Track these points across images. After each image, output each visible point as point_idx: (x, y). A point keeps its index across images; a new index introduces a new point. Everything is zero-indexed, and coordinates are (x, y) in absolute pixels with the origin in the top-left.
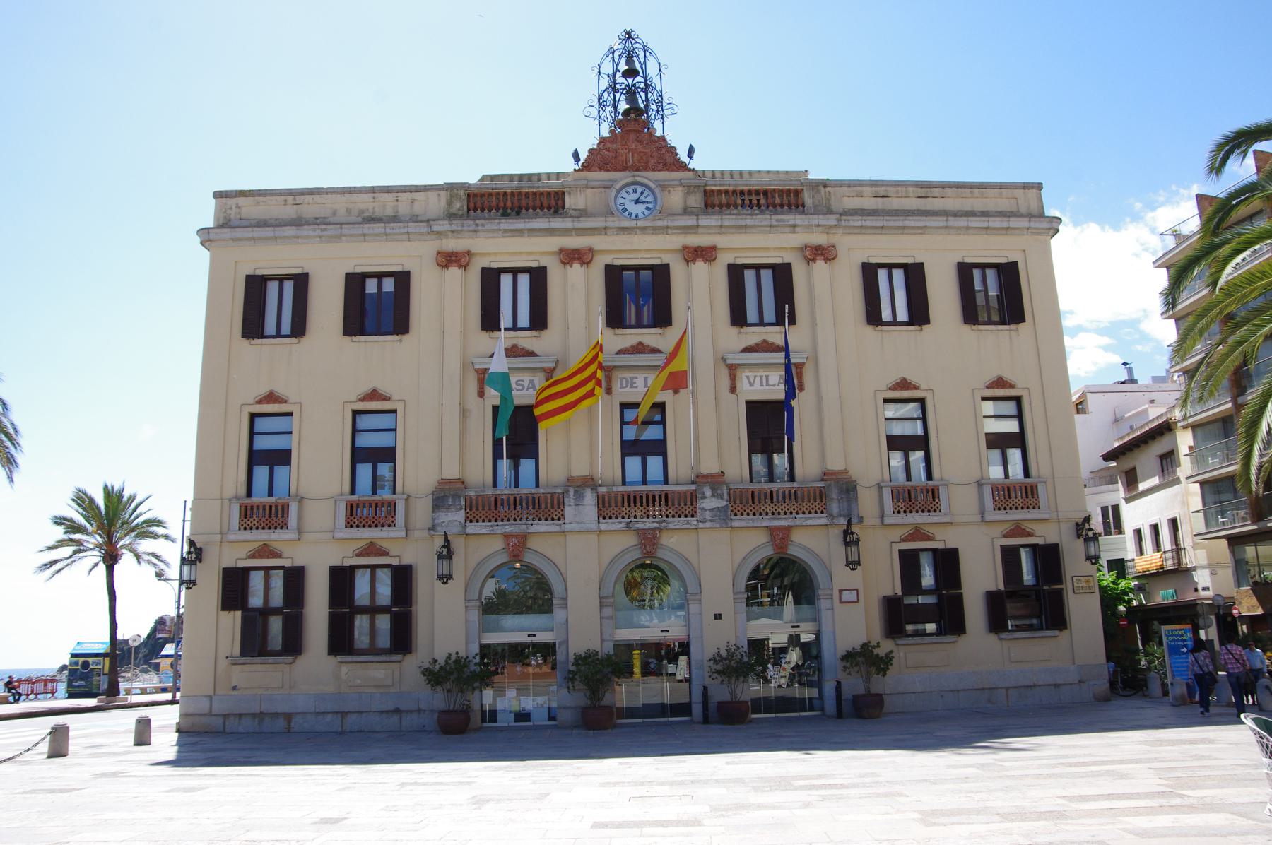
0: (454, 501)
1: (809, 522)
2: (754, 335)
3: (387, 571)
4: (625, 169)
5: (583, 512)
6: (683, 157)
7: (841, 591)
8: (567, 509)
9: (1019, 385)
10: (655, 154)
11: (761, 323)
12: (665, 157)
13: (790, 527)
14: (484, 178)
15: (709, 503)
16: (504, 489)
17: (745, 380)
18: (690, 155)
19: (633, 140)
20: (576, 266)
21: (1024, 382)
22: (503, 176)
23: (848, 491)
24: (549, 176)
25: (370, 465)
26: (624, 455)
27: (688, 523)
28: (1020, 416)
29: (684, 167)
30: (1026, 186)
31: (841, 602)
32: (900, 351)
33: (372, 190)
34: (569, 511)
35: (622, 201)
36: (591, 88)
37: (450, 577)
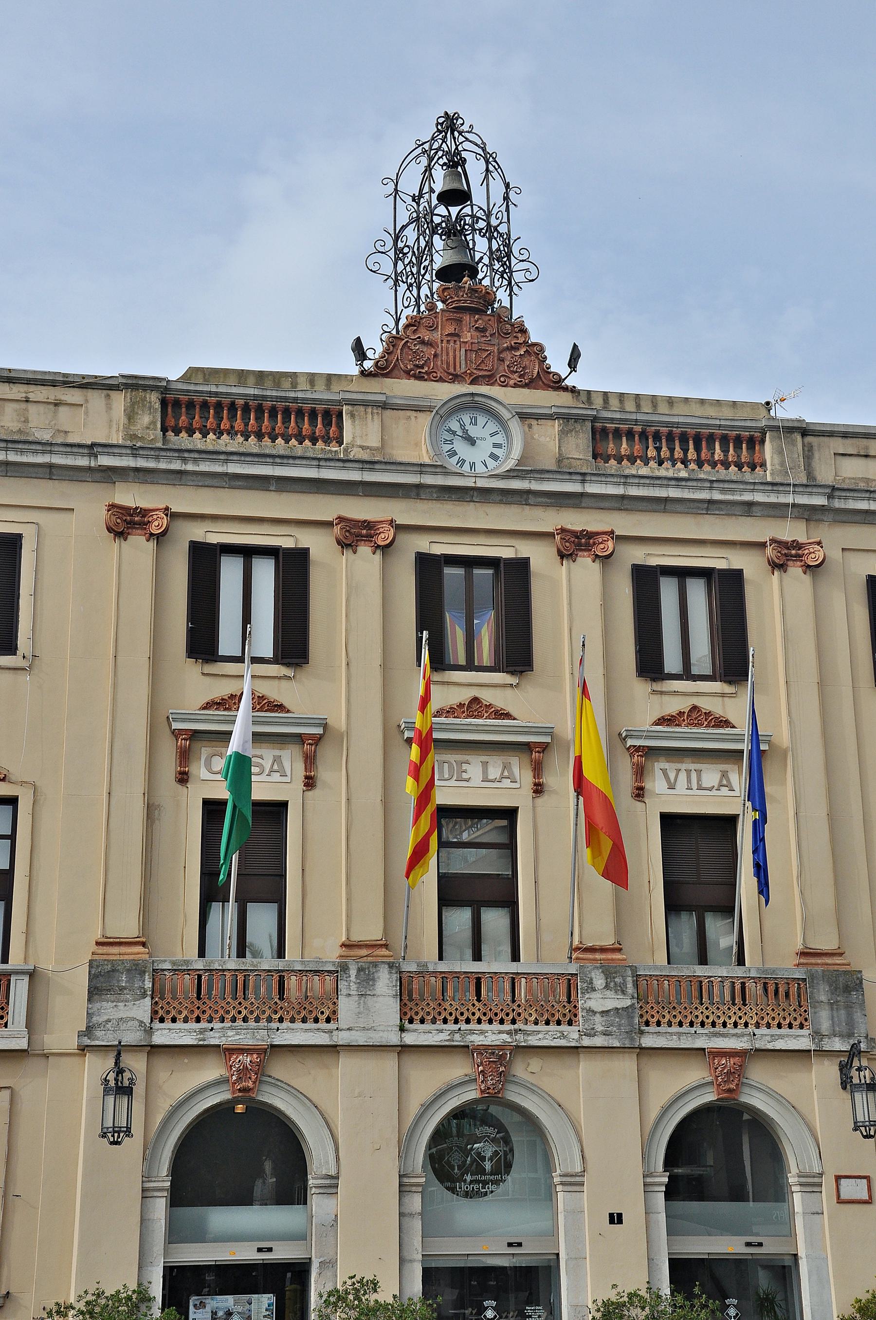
0: (130, 980)
1: (780, 1045)
2: (678, 696)
4: (456, 378)
5: (370, 1012)
6: (558, 364)
7: (838, 1178)
8: (342, 1002)
11: (687, 674)
12: (514, 356)
13: (742, 1054)
14: (192, 373)
15: (600, 1000)
17: (659, 774)
18: (573, 363)
19: (460, 310)
20: (364, 550)
23: (847, 990)
24: (312, 378)
27: (563, 1036)
29: (557, 384)
31: (840, 1201)
34: (346, 1006)
36: (374, 216)
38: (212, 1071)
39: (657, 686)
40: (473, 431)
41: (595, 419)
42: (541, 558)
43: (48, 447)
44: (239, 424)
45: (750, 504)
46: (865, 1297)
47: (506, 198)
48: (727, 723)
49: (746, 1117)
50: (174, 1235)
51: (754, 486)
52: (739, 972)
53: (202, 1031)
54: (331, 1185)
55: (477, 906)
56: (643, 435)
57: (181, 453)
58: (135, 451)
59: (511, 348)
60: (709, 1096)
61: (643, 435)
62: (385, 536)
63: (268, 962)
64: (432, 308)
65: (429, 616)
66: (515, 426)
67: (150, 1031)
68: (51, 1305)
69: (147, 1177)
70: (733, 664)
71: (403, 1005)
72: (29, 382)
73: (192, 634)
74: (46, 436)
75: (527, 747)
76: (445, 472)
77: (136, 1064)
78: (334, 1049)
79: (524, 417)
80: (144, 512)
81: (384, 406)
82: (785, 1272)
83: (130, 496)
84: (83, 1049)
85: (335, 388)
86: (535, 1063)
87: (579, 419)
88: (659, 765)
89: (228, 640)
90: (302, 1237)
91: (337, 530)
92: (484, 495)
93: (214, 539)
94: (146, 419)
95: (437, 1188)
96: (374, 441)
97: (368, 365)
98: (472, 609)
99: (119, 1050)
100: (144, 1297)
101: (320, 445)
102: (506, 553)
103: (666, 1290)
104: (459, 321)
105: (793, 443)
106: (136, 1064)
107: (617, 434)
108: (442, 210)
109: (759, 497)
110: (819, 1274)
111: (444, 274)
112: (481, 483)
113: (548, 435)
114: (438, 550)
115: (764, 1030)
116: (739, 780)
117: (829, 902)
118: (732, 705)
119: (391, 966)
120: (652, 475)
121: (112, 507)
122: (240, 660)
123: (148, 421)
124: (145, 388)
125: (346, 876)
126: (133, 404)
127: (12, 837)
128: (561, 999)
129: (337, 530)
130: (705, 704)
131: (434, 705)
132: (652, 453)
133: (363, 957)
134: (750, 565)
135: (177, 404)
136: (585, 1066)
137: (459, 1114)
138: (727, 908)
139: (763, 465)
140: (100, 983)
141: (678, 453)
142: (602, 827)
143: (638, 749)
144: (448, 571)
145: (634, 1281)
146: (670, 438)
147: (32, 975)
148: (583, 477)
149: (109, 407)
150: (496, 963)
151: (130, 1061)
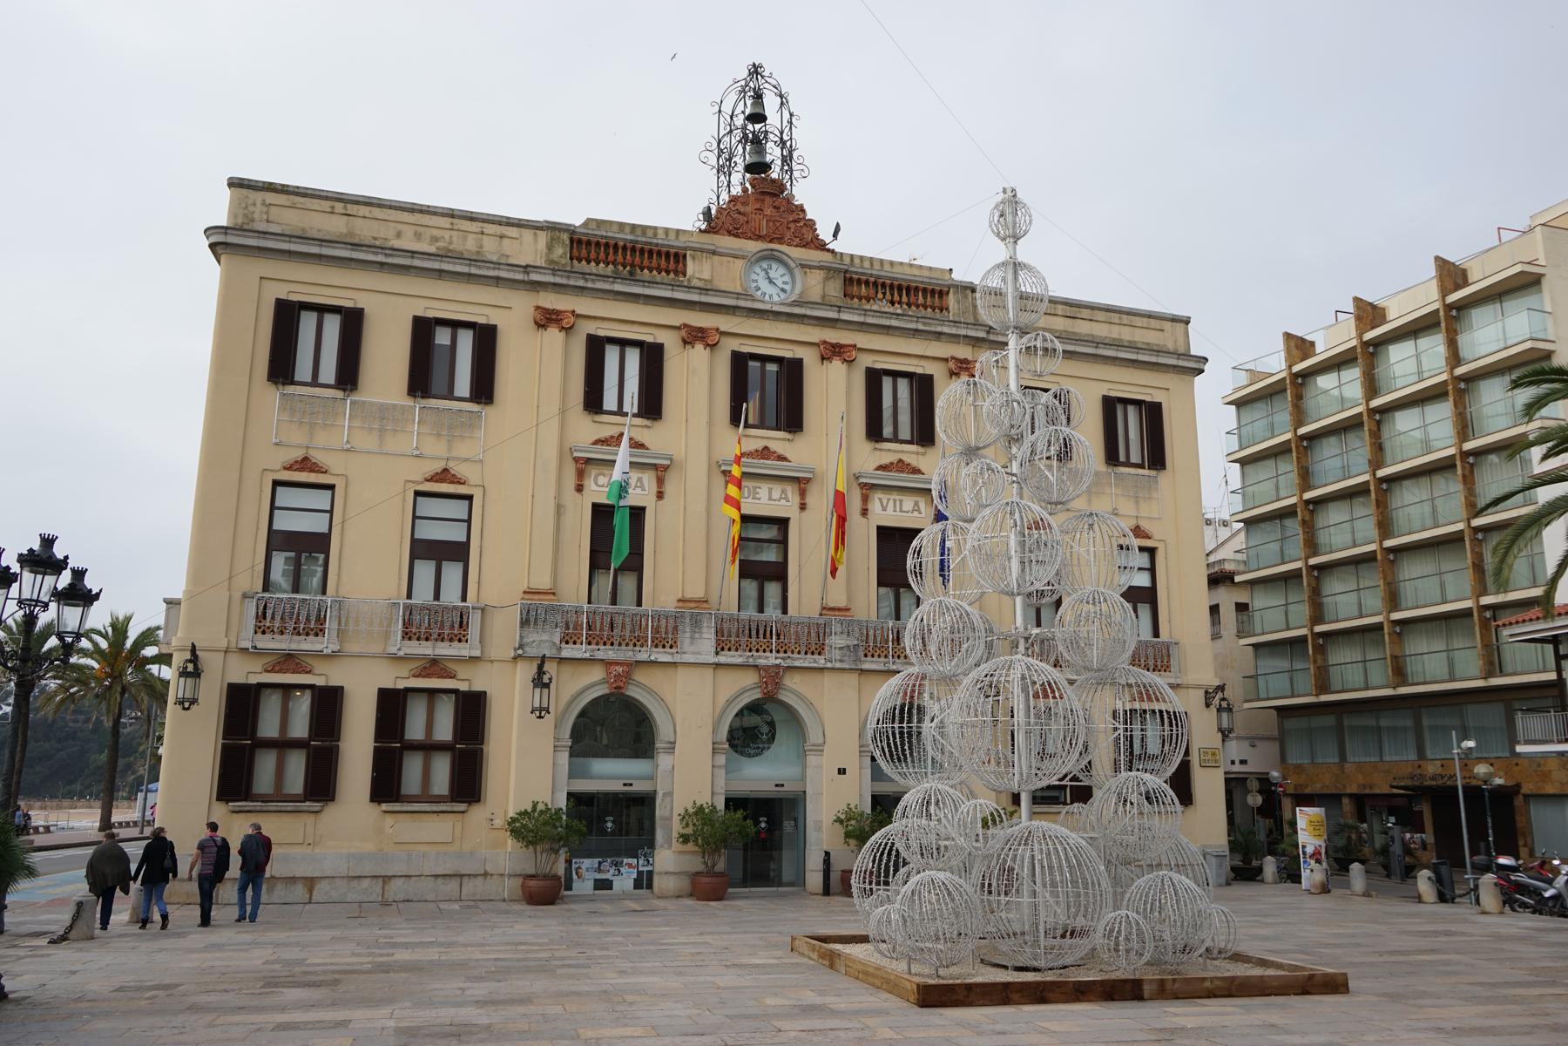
2: (890, 452)
3: (308, 693)
4: (759, 238)
5: (703, 646)
6: (824, 233)
10: (792, 225)
17: (877, 502)
18: (835, 235)
20: (699, 347)
21: (1160, 534)
24: (667, 230)
25: (433, 563)
26: (414, 557)
28: (1152, 570)
29: (822, 246)
30: (1175, 320)
33: (451, 214)
35: (754, 277)
36: (707, 129)
37: (194, 701)
38: (597, 674)
41: (846, 271)
43: (497, 265)
45: (940, 334)
50: (572, 775)
54: (671, 747)
58: (554, 272)
59: (795, 221)
61: (875, 284)
65: (739, 394)
66: (797, 272)
69: (556, 739)
72: (484, 221)
74: (494, 258)
83: (551, 301)
85: (682, 238)
98: (769, 393)
101: (672, 275)
103: (869, 811)
105: (966, 297)
107: (859, 282)
112: (775, 308)
113: (816, 278)
121: (538, 308)
124: (560, 230)
125: (687, 557)
127: (469, 521)
129: (683, 333)
130: (907, 459)
134: (669, 340)
135: (580, 242)
136: (828, 680)
144: (752, 364)
149: (536, 241)
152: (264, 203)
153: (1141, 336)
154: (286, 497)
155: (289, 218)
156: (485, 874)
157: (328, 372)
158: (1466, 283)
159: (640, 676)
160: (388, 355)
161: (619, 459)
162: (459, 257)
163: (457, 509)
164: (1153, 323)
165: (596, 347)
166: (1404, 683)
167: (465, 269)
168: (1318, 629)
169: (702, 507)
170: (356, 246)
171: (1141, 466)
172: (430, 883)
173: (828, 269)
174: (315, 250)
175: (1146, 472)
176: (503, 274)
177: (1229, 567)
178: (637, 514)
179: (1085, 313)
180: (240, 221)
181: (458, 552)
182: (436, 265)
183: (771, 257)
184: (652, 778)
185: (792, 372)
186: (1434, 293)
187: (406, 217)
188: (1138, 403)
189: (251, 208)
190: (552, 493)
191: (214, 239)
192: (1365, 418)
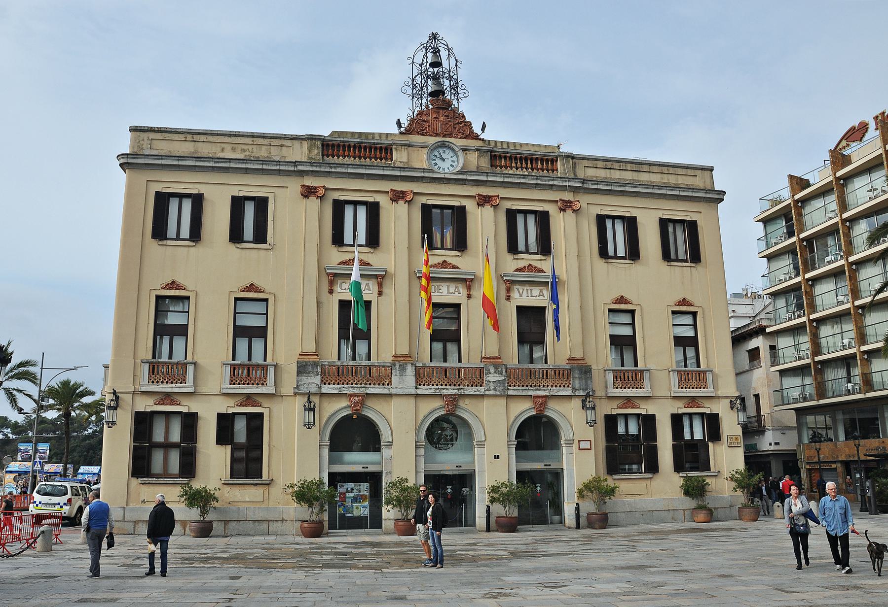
1: (560, 393)
2: (524, 260)
4: (437, 135)
5: (405, 382)
6: (477, 129)
9: (696, 303)
11: (527, 252)
12: (459, 126)
13: (546, 397)
15: (493, 377)
16: (347, 361)
17: (516, 291)
19: (439, 112)
20: (401, 202)
21: (698, 301)
22: (347, 132)
23: (586, 372)
24: (380, 135)
26: (235, 337)
27: (478, 390)
29: (477, 137)
30: (703, 169)
32: (617, 279)
33: (252, 136)
34: (395, 379)
36: (404, 73)
38: (344, 403)
39: (516, 257)
40: (444, 156)
41: (492, 151)
42: (470, 206)
43: (278, 163)
44: (352, 153)
45: (552, 185)
46: (586, 482)
47: (456, 65)
48: (542, 271)
49: (544, 420)
50: (331, 462)
51: (553, 178)
52: (546, 366)
53: (340, 388)
54: (390, 445)
55: (445, 341)
56: (511, 158)
57: (330, 165)
58: (312, 164)
59: (459, 123)
60: (533, 413)
61: (511, 158)
62: (410, 197)
63: (364, 363)
64: (427, 107)
65: (427, 228)
66: (460, 154)
67: (320, 388)
68: (288, 484)
69: (321, 441)
70: (545, 248)
71: (417, 379)
72: (271, 138)
73: (334, 235)
74: (278, 159)
75: (465, 280)
76: (433, 171)
77: (316, 400)
78: (390, 395)
79: (463, 150)
80: (315, 188)
81: (409, 146)
82: (557, 475)
83: (310, 182)
84: (295, 394)
85: (390, 138)
86: (467, 401)
87: (485, 151)
88: (516, 287)
89: (348, 238)
90: (379, 463)
91: (390, 194)
92: (448, 181)
93: (342, 198)
94: (316, 152)
95: (429, 446)
96: (405, 160)
97: (402, 129)
98: (445, 226)
99: (309, 395)
100: (321, 482)
101: (384, 161)
102: (457, 204)
103: (515, 482)
104: (438, 112)
105: (568, 162)
106: (316, 400)
107: (500, 157)
108: (431, 70)
109: (556, 183)
110: (571, 476)
111: (432, 94)
112: (447, 176)
113: (473, 157)
114: (430, 202)
115: (554, 388)
116: (547, 293)
117: (580, 340)
118: (545, 264)
119: (412, 364)
120: (514, 173)
121: (303, 186)
122: (353, 245)
123: (316, 152)
124: (316, 139)
125: (397, 327)
126: (311, 145)
127: (267, 314)
128: (477, 376)
129: (390, 194)
130: (534, 263)
131: (430, 263)
132: (514, 165)
133: (401, 361)
134: (552, 209)
135: (328, 145)
136: (486, 402)
137: (437, 420)
138: (541, 342)
139: (557, 170)
140: (301, 369)
141: (524, 165)
142: (490, 309)
143: (508, 281)
144: (433, 210)
145: (504, 479)
146: (521, 159)
147: (276, 366)
148: (487, 174)
149: (301, 147)
150: (452, 362)
151: (313, 398)
152: (148, 139)
153: (682, 181)
154: (243, 307)
155: (163, 147)
156: (283, 520)
157: (185, 232)
158: (850, 163)
159: (370, 403)
160: (218, 218)
161: (354, 273)
162: (257, 160)
163: (260, 308)
164: (690, 172)
165: (339, 207)
166: (872, 389)
167: (260, 167)
168: (817, 359)
169: (406, 299)
170: (198, 158)
171: (686, 261)
172: (251, 525)
173: (480, 151)
174: (175, 163)
175: (689, 264)
176: (282, 168)
177: (764, 323)
178: (368, 304)
179: (646, 168)
180: (136, 150)
181: (261, 332)
182: (243, 166)
183: (443, 145)
184: (379, 463)
185: (460, 214)
186: (829, 170)
187: (227, 139)
188: (682, 222)
189: (141, 142)
190: (314, 295)
191: (122, 161)
192: (840, 225)
